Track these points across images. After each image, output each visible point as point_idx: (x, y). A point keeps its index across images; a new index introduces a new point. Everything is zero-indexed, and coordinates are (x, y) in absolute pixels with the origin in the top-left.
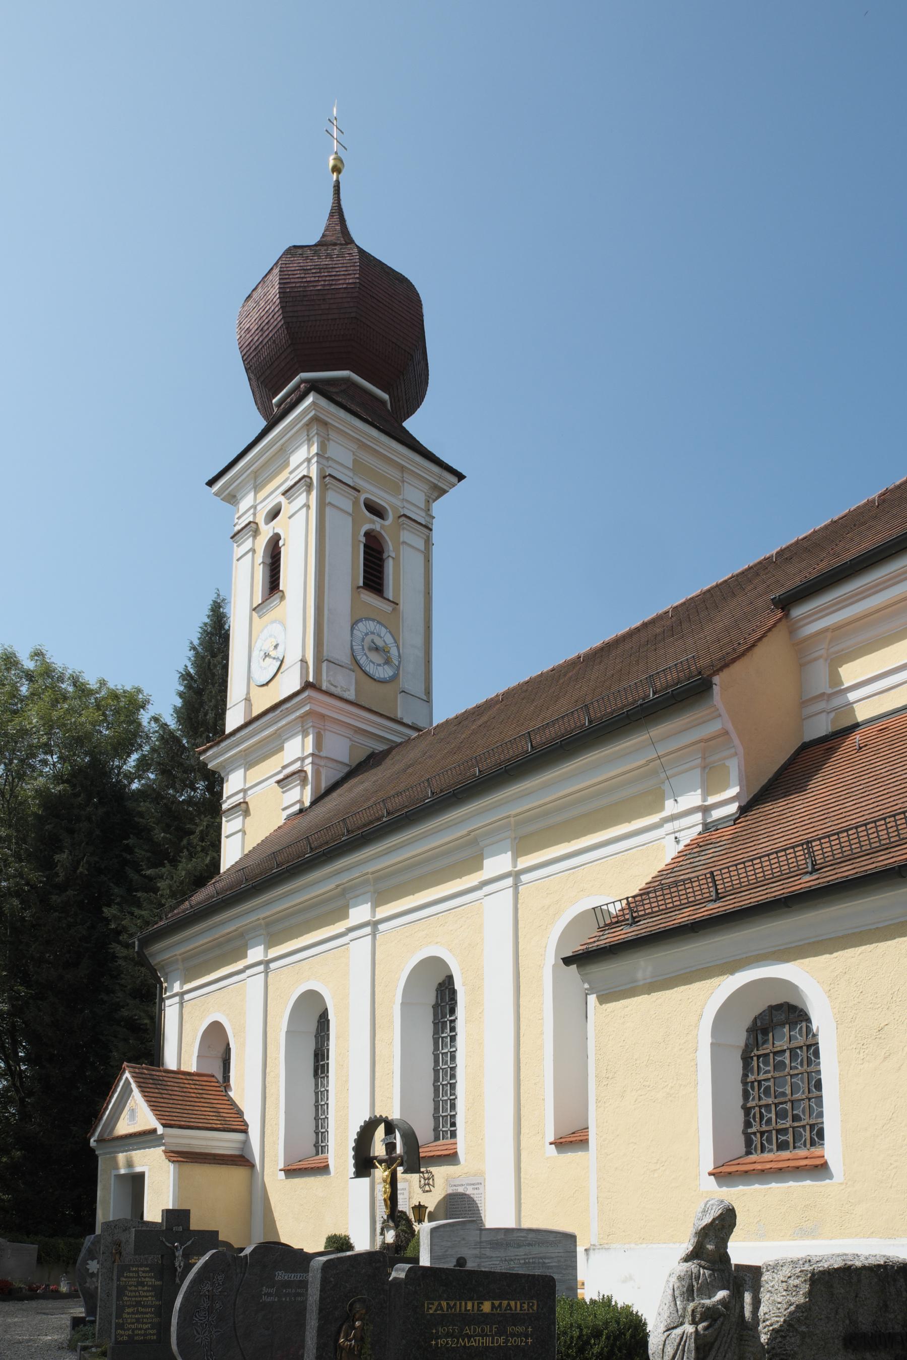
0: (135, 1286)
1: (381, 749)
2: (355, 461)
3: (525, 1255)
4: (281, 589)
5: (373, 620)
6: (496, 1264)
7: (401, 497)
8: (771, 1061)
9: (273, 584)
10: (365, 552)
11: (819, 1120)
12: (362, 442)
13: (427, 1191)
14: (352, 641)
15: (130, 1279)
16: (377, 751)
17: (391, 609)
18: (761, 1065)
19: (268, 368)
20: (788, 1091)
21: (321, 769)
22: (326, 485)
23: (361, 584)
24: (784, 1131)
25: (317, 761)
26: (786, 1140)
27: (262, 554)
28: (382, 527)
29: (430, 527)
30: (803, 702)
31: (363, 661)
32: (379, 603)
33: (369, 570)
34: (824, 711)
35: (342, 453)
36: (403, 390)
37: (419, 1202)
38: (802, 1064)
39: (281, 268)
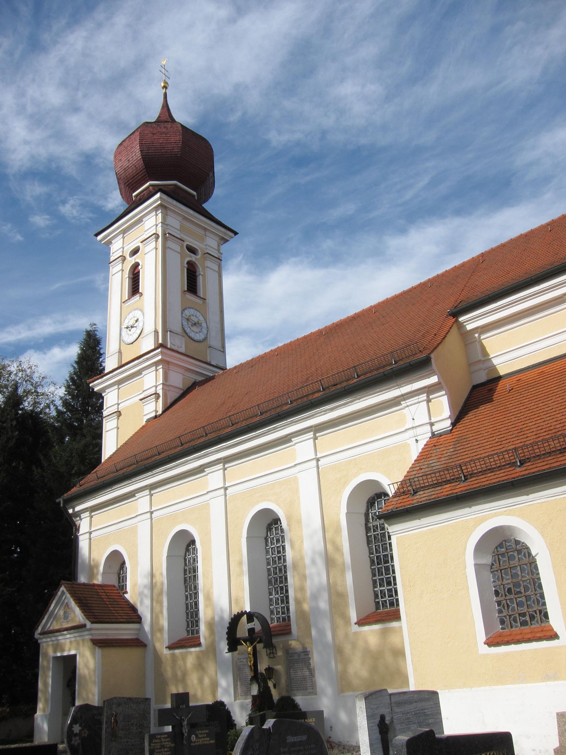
0: (160, 749)
1: (200, 380)
2: (181, 226)
3: (414, 708)
4: (140, 292)
5: (193, 308)
6: (400, 717)
7: (205, 243)
8: (510, 573)
9: (135, 289)
10: (187, 273)
11: (544, 607)
12: (185, 216)
13: (272, 658)
14: (182, 320)
15: (156, 744)
16: (197, 381)
17: (202, 302)
18: (504, 575)
19: (131, 179)
20: (523, 591)
21: (167, 392)
22: (166, 238)
23: (186, 289)
24: (523, 615)
25: (165, 387)
26: (525, 620)
27: (128, 273)
28: (196, 259)
29: (221, 258)
30: (469, 365)
31: (188, 330)
32: (194, 299)
33: (193, 283)
34: (482, 369)
35: (175, 222)
36: (203, 190)
37: (269, 666)
38: (528, 574)
39: (140, 132)
